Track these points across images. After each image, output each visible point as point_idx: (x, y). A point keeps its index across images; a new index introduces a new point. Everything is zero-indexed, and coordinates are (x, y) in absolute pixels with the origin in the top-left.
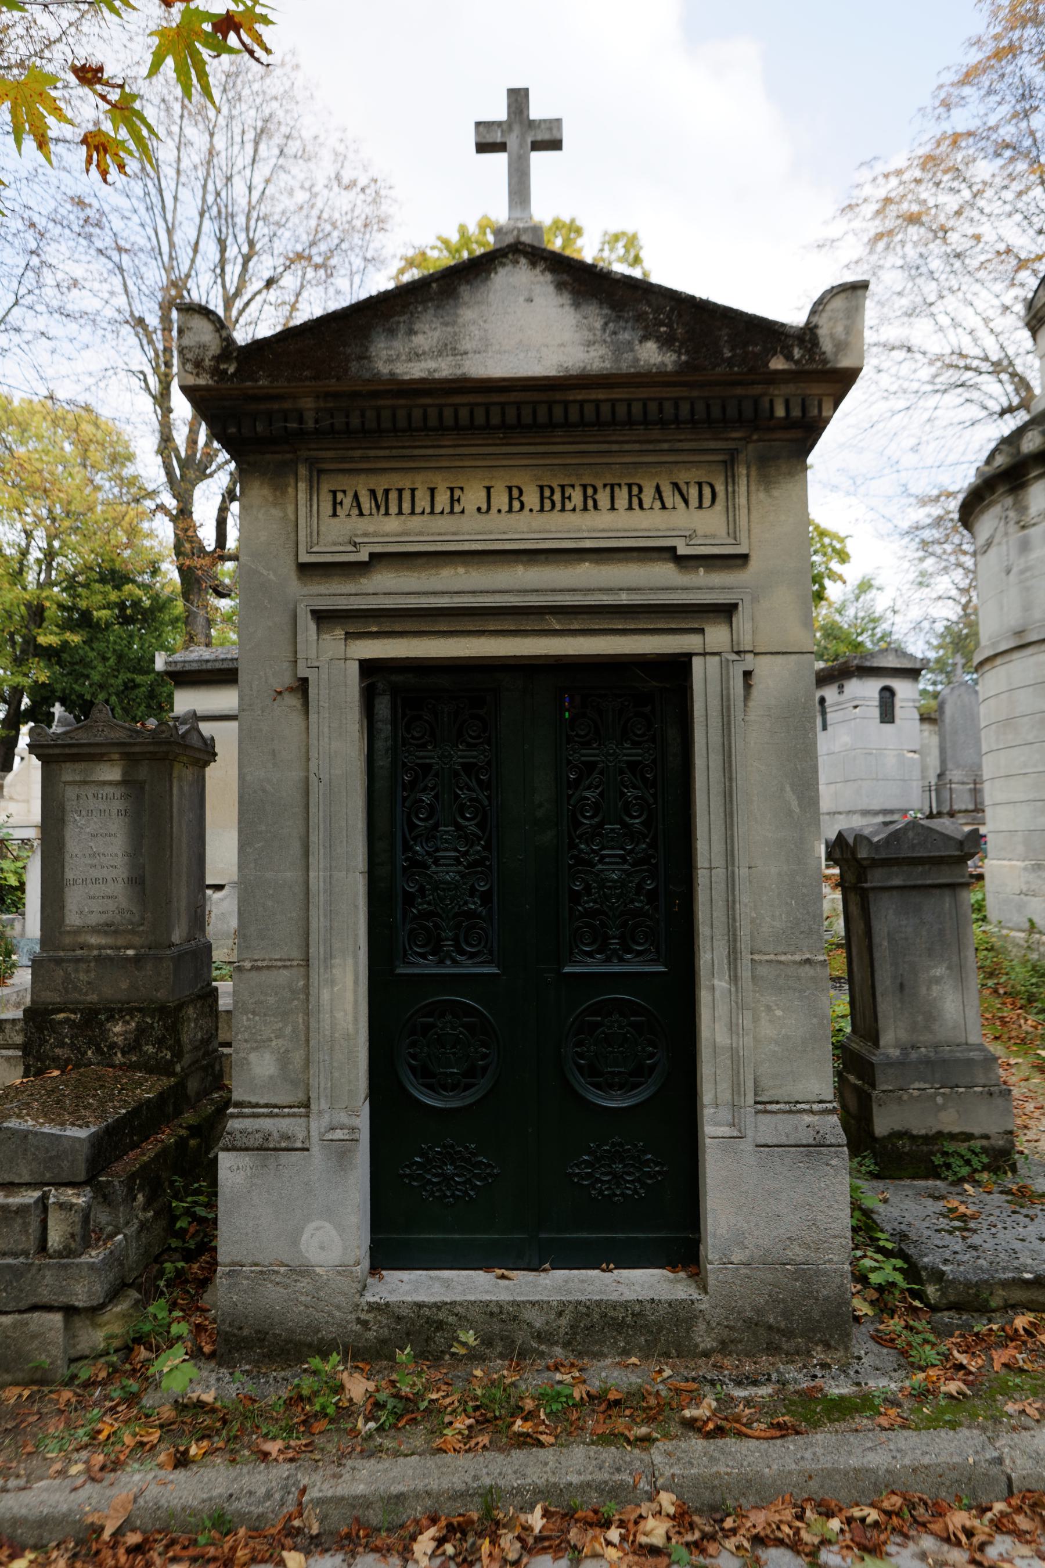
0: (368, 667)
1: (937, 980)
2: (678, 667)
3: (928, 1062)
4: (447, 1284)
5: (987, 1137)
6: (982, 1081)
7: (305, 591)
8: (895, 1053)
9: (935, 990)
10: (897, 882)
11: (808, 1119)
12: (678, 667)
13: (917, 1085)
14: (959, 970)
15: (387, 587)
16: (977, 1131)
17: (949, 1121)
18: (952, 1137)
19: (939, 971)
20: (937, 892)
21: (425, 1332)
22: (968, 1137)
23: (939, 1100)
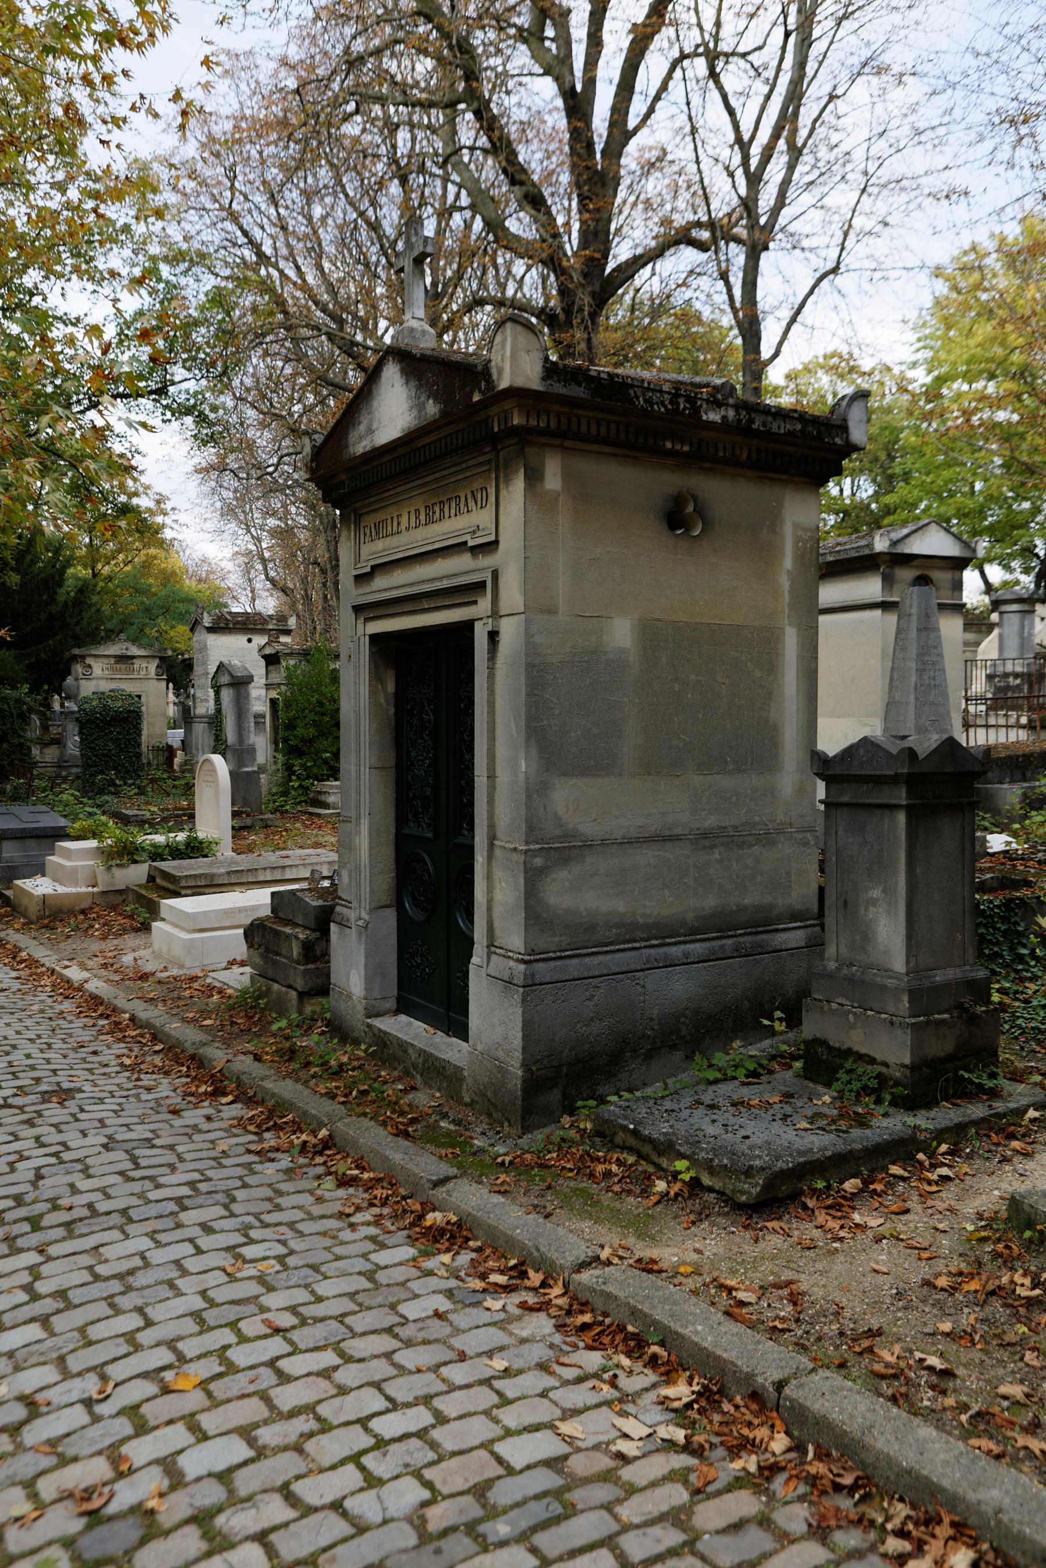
0: (374, 638)
1: (874, 902)
2: (467, 627)
3: (851, 980)
4: (450, 1045)
5: (886, 1065)
6: (892, 1010)
7: (361, 591)
8: (832, 965)
9: (872, 910)
10: (845, 799)
11: (512, 963)
12: (467, 627)
13: (840, 1000)
14: (889, 891)
15: (384, 586)
16: (879, 1057)
17: (857, 1040)
18: (860, 1057)
19: (876, 893)
20: (879, 812)
21: (387, 1051)
22: (872, 1061)
23: (851, 1017)
